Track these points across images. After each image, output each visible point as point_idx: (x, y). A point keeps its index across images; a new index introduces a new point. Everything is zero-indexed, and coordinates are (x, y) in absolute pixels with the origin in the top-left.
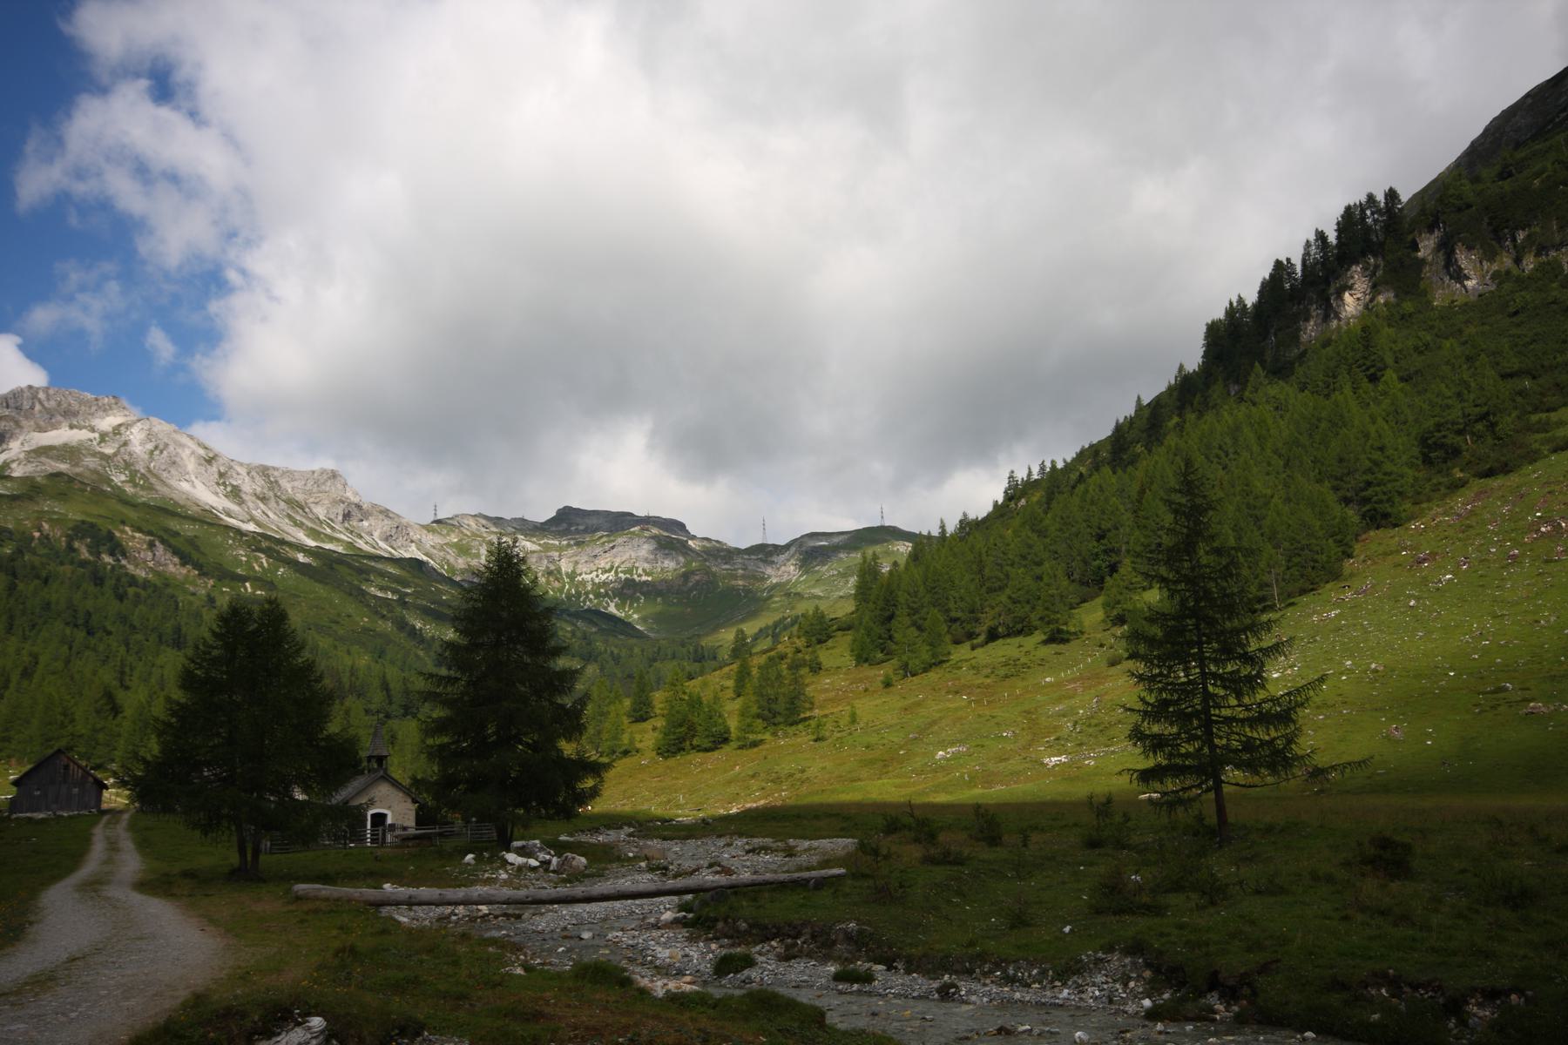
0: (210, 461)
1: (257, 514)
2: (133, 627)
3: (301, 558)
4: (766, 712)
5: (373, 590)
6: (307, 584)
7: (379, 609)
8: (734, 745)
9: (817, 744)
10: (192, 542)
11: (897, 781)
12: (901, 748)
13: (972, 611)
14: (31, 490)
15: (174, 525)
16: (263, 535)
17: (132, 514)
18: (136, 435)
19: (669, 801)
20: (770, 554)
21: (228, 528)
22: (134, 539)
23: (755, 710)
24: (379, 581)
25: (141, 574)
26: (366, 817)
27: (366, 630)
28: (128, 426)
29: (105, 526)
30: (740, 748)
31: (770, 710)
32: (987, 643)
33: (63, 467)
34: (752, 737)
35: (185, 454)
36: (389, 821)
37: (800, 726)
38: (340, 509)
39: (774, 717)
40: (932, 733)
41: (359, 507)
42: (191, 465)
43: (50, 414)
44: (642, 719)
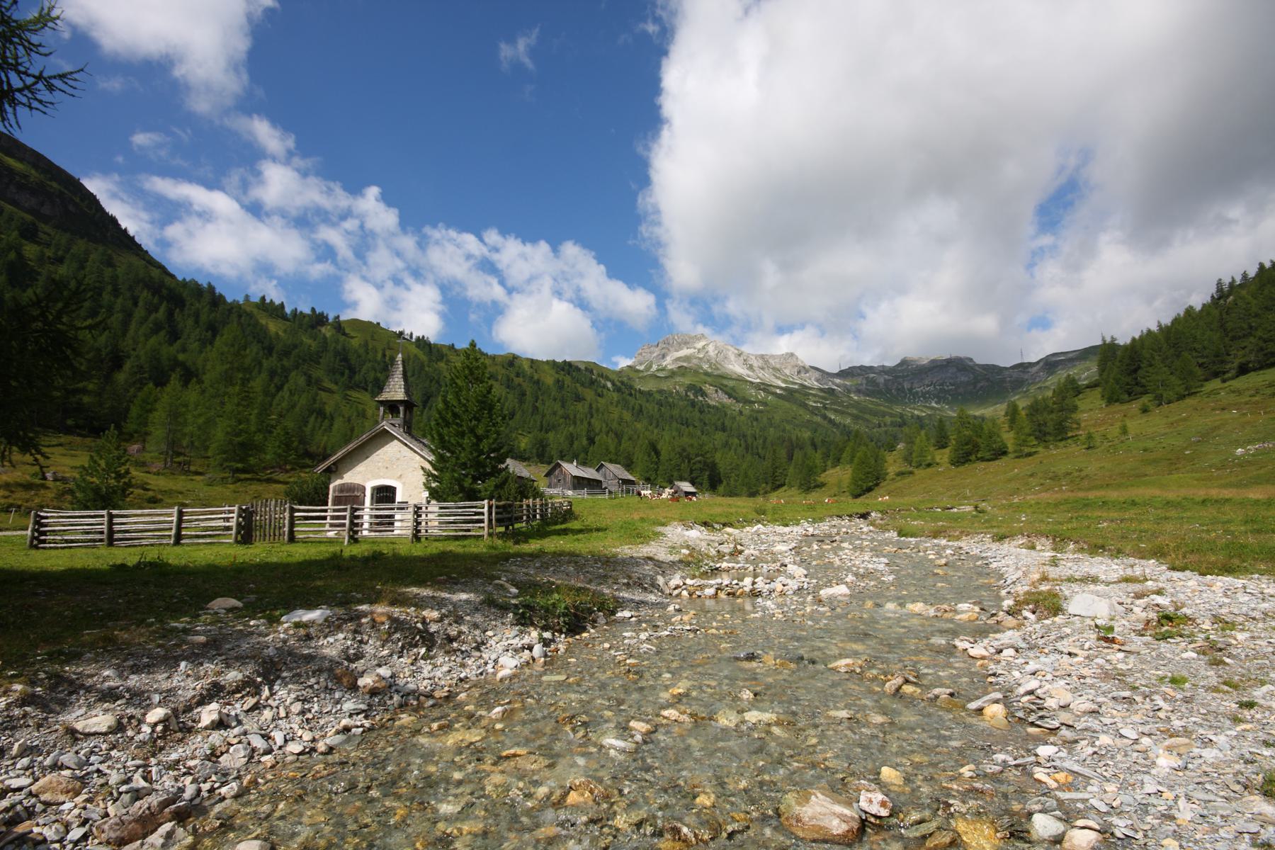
0: (740, 355)
1: (760, 375)
2: (705, 423)
3: (778, 391)
4: (1037, 433)
5: (811, 403)
6: (781, 402)
7: (814, 411)
8: (1011, 456)
9: (1090, 451)
10: (733, 388)
11: (1198, 475)
12: (1186, 449)
13: (1217, 356)
14: (673, 374)
15: (725, 382)
16: (763, 384)
17: (709, 379)
18: (711, 348)
19: (959, 494)
20: (1027, 367)
21: (747, 381)
22: (709, 389)
23: (1027, 430)
24: (814, 399)
25: (712, 403)
26: (328, 488)
27: (808, 421)
28: (707, 345)
29: (699, 385)
30: (1017, 457)
31: (1040, 432)
32: (1237, 376)
33: (685, 364)
34: (1027, 450)
35: (730, 353)
36: (399, 498)
37: (1069, 441)
38: (796, 370)
39: (1045, 435)
40: (1219, 436)
41: (804, 367)
42: (732, 358)
43: (680, 344)
44: (944, 447)
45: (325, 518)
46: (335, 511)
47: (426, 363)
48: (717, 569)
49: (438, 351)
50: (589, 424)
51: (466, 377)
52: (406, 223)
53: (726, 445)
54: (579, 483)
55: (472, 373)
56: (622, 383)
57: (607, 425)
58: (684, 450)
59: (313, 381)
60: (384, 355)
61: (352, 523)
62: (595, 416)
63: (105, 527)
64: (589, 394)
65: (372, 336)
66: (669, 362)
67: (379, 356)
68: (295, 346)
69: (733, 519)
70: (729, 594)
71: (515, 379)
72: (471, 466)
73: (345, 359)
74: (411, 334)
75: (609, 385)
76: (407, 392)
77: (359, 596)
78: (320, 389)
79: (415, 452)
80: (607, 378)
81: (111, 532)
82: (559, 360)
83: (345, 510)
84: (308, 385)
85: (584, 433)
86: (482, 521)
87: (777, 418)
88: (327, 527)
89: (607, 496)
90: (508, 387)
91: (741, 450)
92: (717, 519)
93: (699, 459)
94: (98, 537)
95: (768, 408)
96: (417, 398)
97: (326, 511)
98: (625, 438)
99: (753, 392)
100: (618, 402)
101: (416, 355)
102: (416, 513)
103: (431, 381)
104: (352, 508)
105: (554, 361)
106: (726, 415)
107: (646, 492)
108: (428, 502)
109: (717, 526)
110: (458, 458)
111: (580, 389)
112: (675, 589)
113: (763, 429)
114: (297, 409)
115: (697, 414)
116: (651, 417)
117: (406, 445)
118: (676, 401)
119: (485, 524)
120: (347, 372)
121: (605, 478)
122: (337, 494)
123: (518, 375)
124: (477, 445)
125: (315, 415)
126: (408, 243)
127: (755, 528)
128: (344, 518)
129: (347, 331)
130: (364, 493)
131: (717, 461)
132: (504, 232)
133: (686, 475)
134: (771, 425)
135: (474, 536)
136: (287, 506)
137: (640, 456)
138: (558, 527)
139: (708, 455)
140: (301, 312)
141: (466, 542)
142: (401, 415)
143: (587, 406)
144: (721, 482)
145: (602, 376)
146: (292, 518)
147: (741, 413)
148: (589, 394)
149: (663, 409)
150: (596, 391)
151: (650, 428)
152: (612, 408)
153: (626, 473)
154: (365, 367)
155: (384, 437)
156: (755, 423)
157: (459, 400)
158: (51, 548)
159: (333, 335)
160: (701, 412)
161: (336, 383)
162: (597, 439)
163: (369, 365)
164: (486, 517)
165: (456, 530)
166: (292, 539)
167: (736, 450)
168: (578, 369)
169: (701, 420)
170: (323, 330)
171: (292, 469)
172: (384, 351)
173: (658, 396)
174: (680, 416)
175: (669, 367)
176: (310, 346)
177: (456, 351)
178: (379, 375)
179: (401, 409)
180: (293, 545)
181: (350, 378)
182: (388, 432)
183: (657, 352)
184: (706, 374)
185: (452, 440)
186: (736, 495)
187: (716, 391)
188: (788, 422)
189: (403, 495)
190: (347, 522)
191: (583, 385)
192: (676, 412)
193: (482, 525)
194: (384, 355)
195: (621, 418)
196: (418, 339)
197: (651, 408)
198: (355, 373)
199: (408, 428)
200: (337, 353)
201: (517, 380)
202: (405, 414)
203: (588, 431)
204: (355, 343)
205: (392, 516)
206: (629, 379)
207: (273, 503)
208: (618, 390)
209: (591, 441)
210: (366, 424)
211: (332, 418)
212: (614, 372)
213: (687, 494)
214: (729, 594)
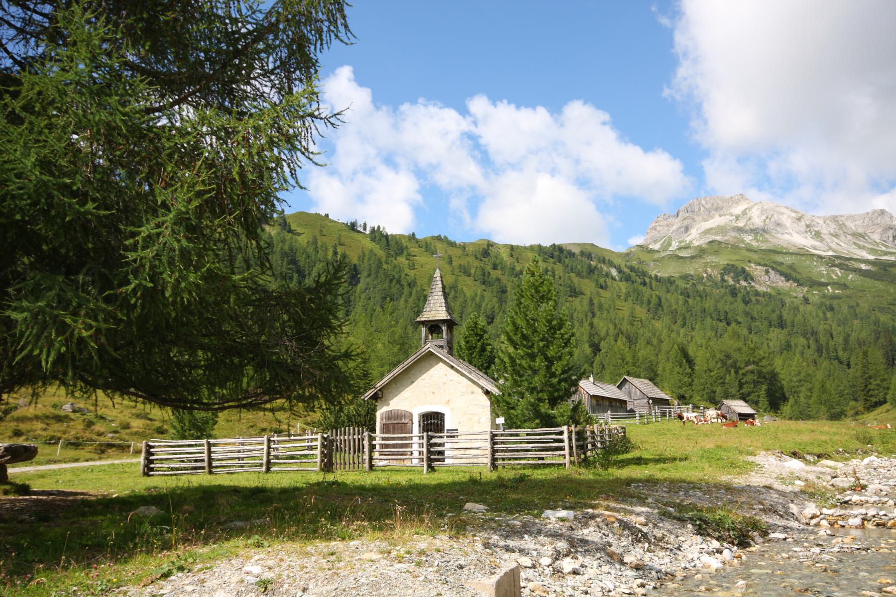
0: (799, 219)
1: (833, 245)
3: (863, 267)
6: (869, 282)
10: (791, 267)
14: (701, 252)
15: (779, 259)
17: (754, 256)
22: (756, 270)
25: (762, 289)
28: (750, 209)
29: (739, 265)
33: (718, 238)
36: (448, 426)
46: (384, 439)
47: (383, 260)
48: (846, 502)
49: (397, 243)
50: (591, 325)
52: (378, 100)
53: (788, 347)
54: (598, 405)
55: (537, 292)
56: (632, 269)
57: (615, 326)
58: (728, 356)
60: (335, 253)
62: (598, 314)
63: (205, 456)
64: (588, 286)
65: (321, 231)
66: (695, 237)
69: (830, 449)
70: (878, 525)
71: (492, 272)
73: (293, 261)
74: (365, 225)
75: (614, 272)
76: (449, 309)
79: (463, 375)
80: (611, 264)
81: (210, 460)
82: (546, 243)
85: (585, 338)
86: (562, 449)
87: (864, 306)
89: (637, 421)
90: (484, 283)
91: (811, 353)
92: (809, 448)
93: (750, 368)
94: (199, 464)
95: (847, 292)
96: (456, 316)
98: (641, 342)
99: (823, 269)
100: (628, 295)
101: (371, 251)
103: (391, 281)
105: (540, 246)
106: (783, 305)
107: (689, 415)
109: (808, 457)
111: (576, 280)
112: (812, 518)
113: (843, 322)
115: (740, 306)
116: (674, 313)
117: (452, 367)
118: (708, 289)
119: (567, 452)
120: (296, 275)
121: (630, 397)
122: (385, 421)
123: (495, 267)
126: (382, 121)
127: (867, 460)
129: (293, 228)
131: (778, 370)
132: (494, 100)
133: (733, 391)
134: (856, 316)
137: (665, 366)
138: (621, 457)
139: (764, 363)
143: (586, 302)
144: (785, 399)
145: (604, 261)
147: (806, 300)
148: (588, 286)
149: (690, 301)
150: (597, 281)
151: (675, 327)
152: (619, 303)
153: (657, 390)
154: (315, 269)
155: (430, 358)
156: (829, 315)
158: (159, 475)
159: (279, 234)
160: (746, 303)
162: (603, 345)
164: (566, 444)
166: (371, 467)
167: (802, 353)
168: (571, 255)
169: (747, 314)
172: (335, 247)
173: (681, 284)
174: (716, 309)
175: (696, 243)
177: (417, 241)
179: (444, 328)
183: (677, 223)
184: (750, 250)
185: (524, 362)
186: (809, 417)
187: (767, 272)
188: (882, 310)
191: (579, 274)
192: (709, 304)
193: (562, 453)
194: (335, 253)
195: (633, 316)
196: (373, 231)
197: (674, 300)
198: (304, 277)
200: (284, 254)
201: (494, 274)
203: (591, 335)
204: (302, 240)
206: (641, 263)
208: (628, 279)
209: (596, 349)
212: (619, 255)
213: (744, 417)
214: (878, 525)
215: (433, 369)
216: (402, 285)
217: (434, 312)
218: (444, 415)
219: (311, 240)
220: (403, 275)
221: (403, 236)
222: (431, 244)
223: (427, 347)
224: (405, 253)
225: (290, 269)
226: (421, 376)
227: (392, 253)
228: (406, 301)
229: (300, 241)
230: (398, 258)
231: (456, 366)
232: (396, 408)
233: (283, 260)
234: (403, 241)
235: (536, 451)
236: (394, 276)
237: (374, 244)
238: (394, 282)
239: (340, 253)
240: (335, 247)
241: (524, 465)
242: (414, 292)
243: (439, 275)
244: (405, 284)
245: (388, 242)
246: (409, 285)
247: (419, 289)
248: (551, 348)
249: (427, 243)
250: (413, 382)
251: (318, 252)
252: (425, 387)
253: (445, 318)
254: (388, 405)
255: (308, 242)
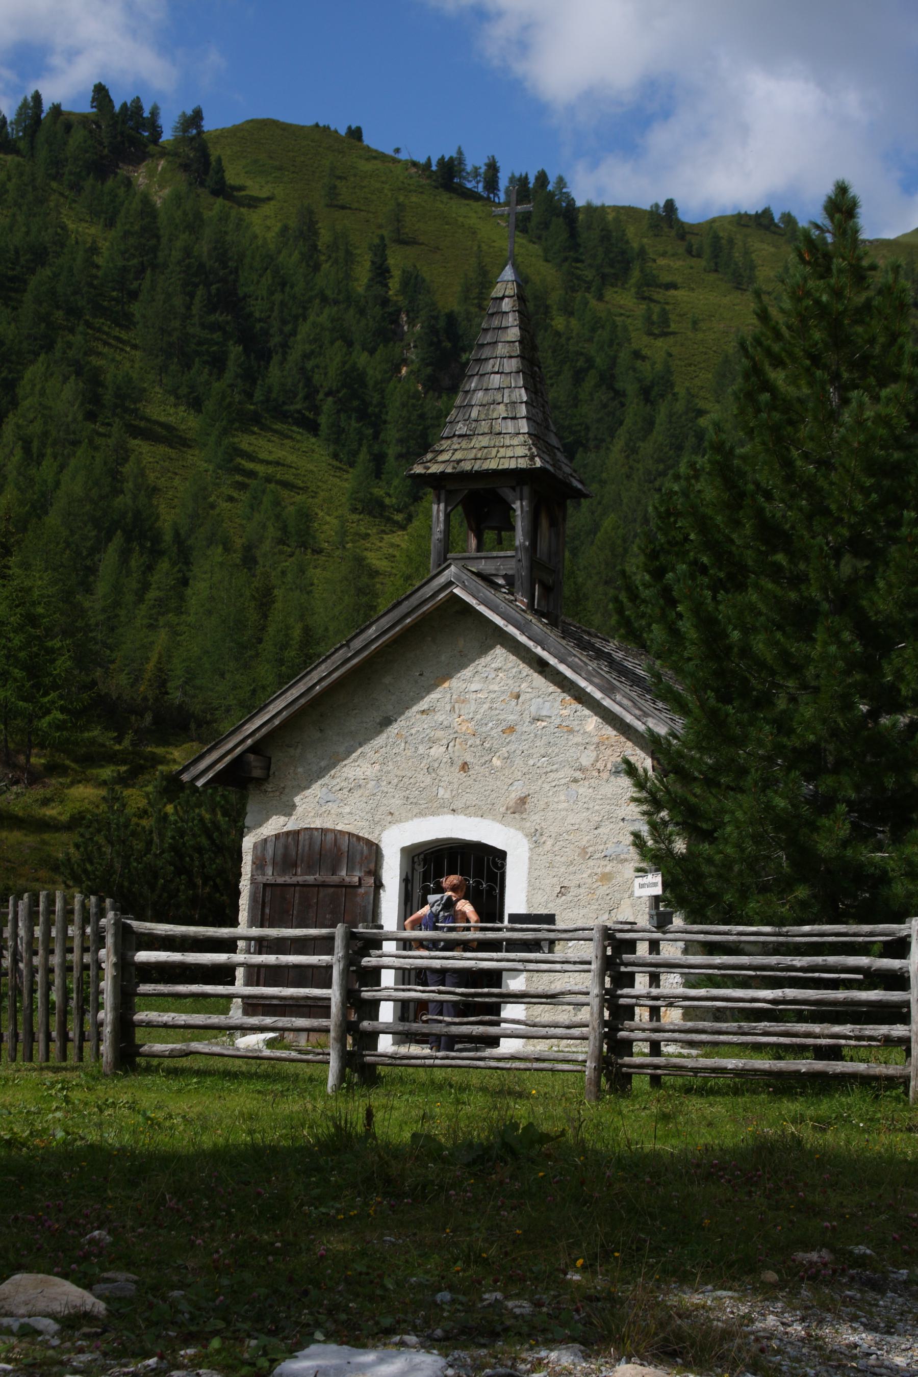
45: (224, 974)
47: (555, 298)
49: (606, 237)
51: (815, 360)
59: (108, 397)
60: (381, 272)
61: (351, 997)
65: (333, 191)
67: (363, 273)
68: (40, 256)
72: (840, 765)
74: (493, 168)
77: (521, 1306)
78: (135, 432)
79: (582, 697)
83: (324, 945)
84: (91, 416)
88: (236, 1015)
94: (563, 1014)
97: (229, 945)
102: (609, 965)
103: (578, 377)
104: (351, 937)
108: (662, 922)
110: (783, 725)
114: (53, 519)
117: (541, 666)
120: (235, 350)
122: (269, 875)
124: (870, 666)
125: (118, 539)
128: (321, 976)
129: (232, 177)
130: (375, 874)
135: (865, 1080)
136: (108, 921)
140: (56, 109)
141: (825, 1107)
142: (520, 538)
146: (125, 966)
154: (304, 329)
157: (788, 463)
159: (178, 199)
161: (196, 404)
163: (321, 316)
165: (779, 1052)
170: (140, 177)
171: (52, 769)
172: (380, 251)
176: (94, 250)
177: (683, 232)
178: (362, 359)
179: (520, 508)
180: (134, 1080)
181: (250, 376)
182: (467, 609)
185: (759, 645)
189: (533, 886)
190: (334, 994)
193: (323, 1022)
194: (381, 272)
196: (520, 183)
198: (265, 356)
199: (547, 590)
202: (533, 533)
205: (494, 978)
207: (23, 905)
210: (316, 574)
211: (184, 555)
215: (467, 672)
216: (619, 394)
217: (484, 441)
218: (502, 855)
219: (293, 223)
220: (624, 356)
221: (631, 213)
222: (731, 241)
223: (441, 580)
224: (636, 274)
225: (214, 327)
226: (420, 698)
227: (589, 274)
228: (631, 450)
229: (257, 230)
230: (609, 294)
231: (553, 661)
232: (317, 824)
233: (192, 295)
234: (631, 231)
235: (801, 1017)
236: (590, 361)
237: (521, 240)
238: (591, 381)
239: (396, 273)
240: (380, 251)
241: (739, 1073)
242: (661, 417)
243: (511, 290)
244: (630, 388)
245: (573, 233)
246: (646, 393)
247: (679, 407)
248: (881, 584)
249: (716, 238)
250: (387, 722)
251: (317, 267)
252: (433, 741)
253: (523, 464)
254: (288, 809)
255: (285, 228)
